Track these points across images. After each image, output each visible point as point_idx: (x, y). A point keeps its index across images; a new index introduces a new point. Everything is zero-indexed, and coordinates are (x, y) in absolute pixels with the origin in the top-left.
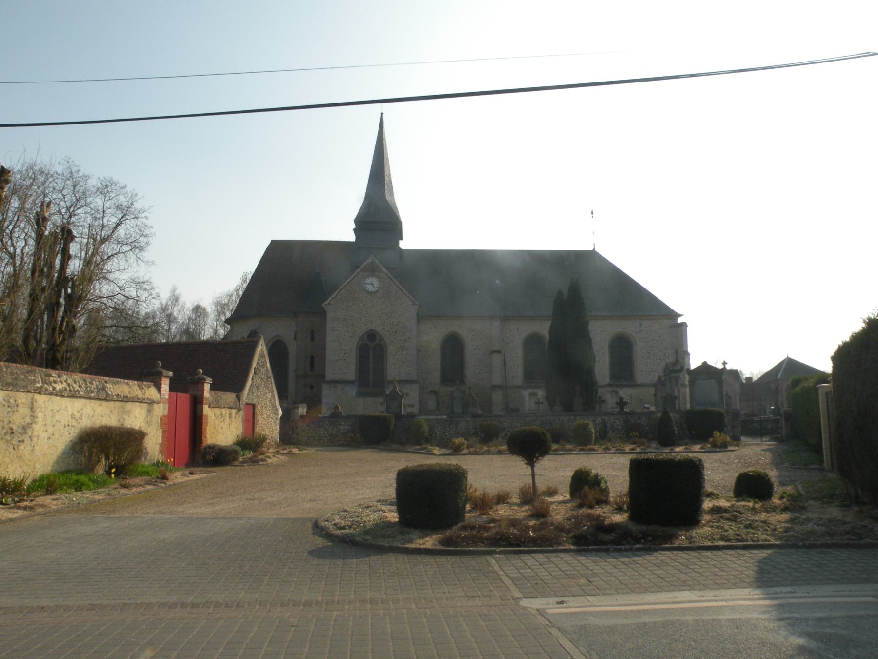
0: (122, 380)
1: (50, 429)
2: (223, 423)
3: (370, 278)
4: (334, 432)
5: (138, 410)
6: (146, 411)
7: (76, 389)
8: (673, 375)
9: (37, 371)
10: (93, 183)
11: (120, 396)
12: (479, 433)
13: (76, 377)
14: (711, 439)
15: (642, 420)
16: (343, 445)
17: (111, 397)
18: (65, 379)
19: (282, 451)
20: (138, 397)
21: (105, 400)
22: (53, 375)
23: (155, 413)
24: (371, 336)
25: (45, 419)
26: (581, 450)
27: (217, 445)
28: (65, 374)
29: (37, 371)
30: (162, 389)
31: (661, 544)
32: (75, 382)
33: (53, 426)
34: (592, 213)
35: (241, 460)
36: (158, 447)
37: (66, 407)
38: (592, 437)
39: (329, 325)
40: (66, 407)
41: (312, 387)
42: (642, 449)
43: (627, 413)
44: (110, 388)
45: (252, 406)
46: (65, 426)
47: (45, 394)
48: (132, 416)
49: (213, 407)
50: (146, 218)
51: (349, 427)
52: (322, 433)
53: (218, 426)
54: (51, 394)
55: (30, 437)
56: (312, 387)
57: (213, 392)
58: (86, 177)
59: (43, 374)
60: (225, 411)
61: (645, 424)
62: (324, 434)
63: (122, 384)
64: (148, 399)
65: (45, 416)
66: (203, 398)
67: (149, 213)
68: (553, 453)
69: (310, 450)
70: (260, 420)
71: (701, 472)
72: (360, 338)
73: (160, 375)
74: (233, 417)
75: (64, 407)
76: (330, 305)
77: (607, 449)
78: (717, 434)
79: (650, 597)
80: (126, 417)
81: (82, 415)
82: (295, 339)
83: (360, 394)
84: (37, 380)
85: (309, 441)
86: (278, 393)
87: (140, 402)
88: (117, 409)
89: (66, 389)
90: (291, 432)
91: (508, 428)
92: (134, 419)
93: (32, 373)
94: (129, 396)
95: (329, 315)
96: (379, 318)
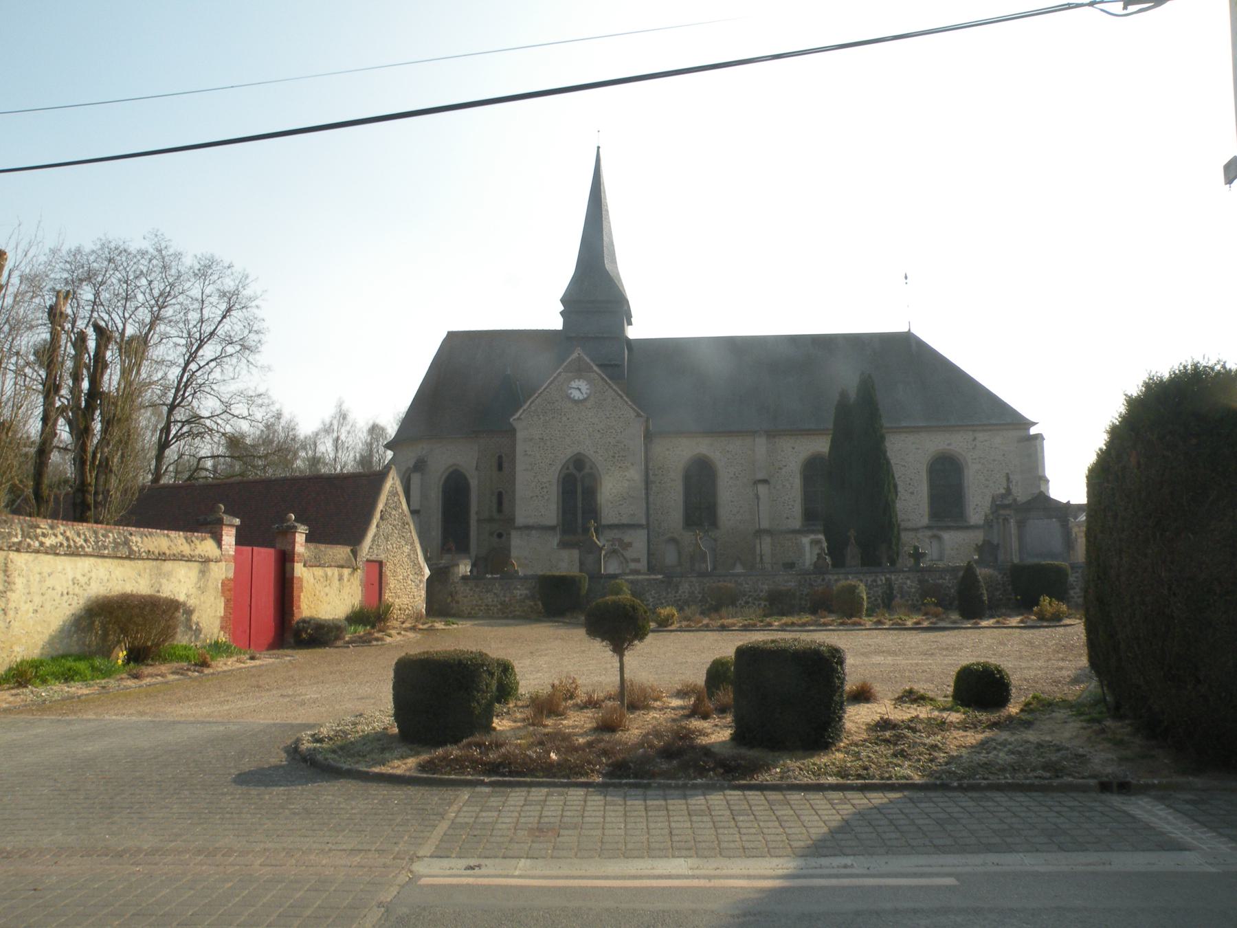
0: (158, 531)
1: (37, 600)
2: (328, 587)
3: (576, 380)
4: (507, 599)
5: (183, 572)
6: (197, 572)
7: (78, 545)
8: (1002, 512)
9: (16, 521)
10: (188, 261)
11: (153, 553)
12: (709, 599)
13: (81, 528)
14: (1035, 609)
15: (945, 579)
16: (514, 618)
17: (137, 555)
18: (62, 531)
19: (421, 627)
20: (184, 553)
21: (128, 558)
22: (42, 526)
23: (212, 574)
24: (579, 462)
25: (28, 584)
26: (842, 624)
27: (314, 619)
28: (62, 525)
29: (16, 521)
30: (223, 543)
31: (734, 778)
32: (79, 535)
33: (42, 594)
34: (906, 278)
35: (347, 639)
36: (218, 623)
37: (64, 569)
38: (862, 605)
39: (520, 448)
40: (64, 569)
41: (500, 536)
42: (931, 623)
43: (923, 570)
44: (137, 542)
45: (377, 564)
46: (62, 595)
47: (27, 552)
48: (173, 579)
49: (312, 566)
50: (257, 307)
51: (527, 592)
52: (490, 600)
53: (320, 592)
54: (37, 552)
55: (3, 610)
56: (500, 536)
57: (312, 546)
58: (178, 256)
59: (25, 525)
60: (333, 572)
61: (950, 585)
62: (493, 601)
63: (158, 536)
64: (200, 556)
65: (28, 581)
66: (294, 554)
67: (263, 300)
68: (800, 629)
69: (462, 624)
70: (392, 583)
71: (836, 671)
72: (563, 466)
73: (220, 522)
74: (346, 580)
75: (60, 568)
76: (521, 419)
77: (879, 622)
78: (1045, 601)
79: (595, 867)
80: (164, 581)
81: (89, 579)
82: (477, 468)
83: (564, 545)
84: (14, 533)
85: (473, 612)
86: (421, 544)
87: (186, 561)
88: (148, 571)
89: (61, 545)
90: (449, 600)
91: (750, 592)
92: (177, 584)
93: (7, 524)
94: (168, 552)
95: (520, 435)
96: (589, 436)
